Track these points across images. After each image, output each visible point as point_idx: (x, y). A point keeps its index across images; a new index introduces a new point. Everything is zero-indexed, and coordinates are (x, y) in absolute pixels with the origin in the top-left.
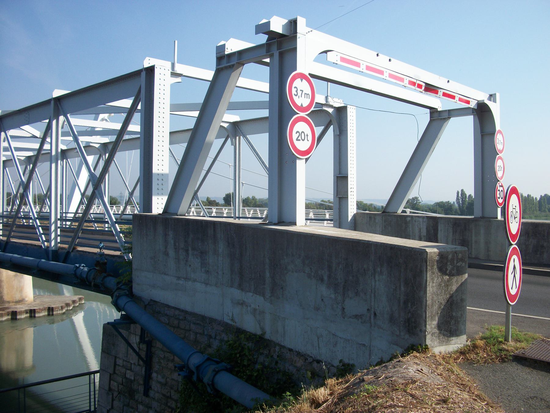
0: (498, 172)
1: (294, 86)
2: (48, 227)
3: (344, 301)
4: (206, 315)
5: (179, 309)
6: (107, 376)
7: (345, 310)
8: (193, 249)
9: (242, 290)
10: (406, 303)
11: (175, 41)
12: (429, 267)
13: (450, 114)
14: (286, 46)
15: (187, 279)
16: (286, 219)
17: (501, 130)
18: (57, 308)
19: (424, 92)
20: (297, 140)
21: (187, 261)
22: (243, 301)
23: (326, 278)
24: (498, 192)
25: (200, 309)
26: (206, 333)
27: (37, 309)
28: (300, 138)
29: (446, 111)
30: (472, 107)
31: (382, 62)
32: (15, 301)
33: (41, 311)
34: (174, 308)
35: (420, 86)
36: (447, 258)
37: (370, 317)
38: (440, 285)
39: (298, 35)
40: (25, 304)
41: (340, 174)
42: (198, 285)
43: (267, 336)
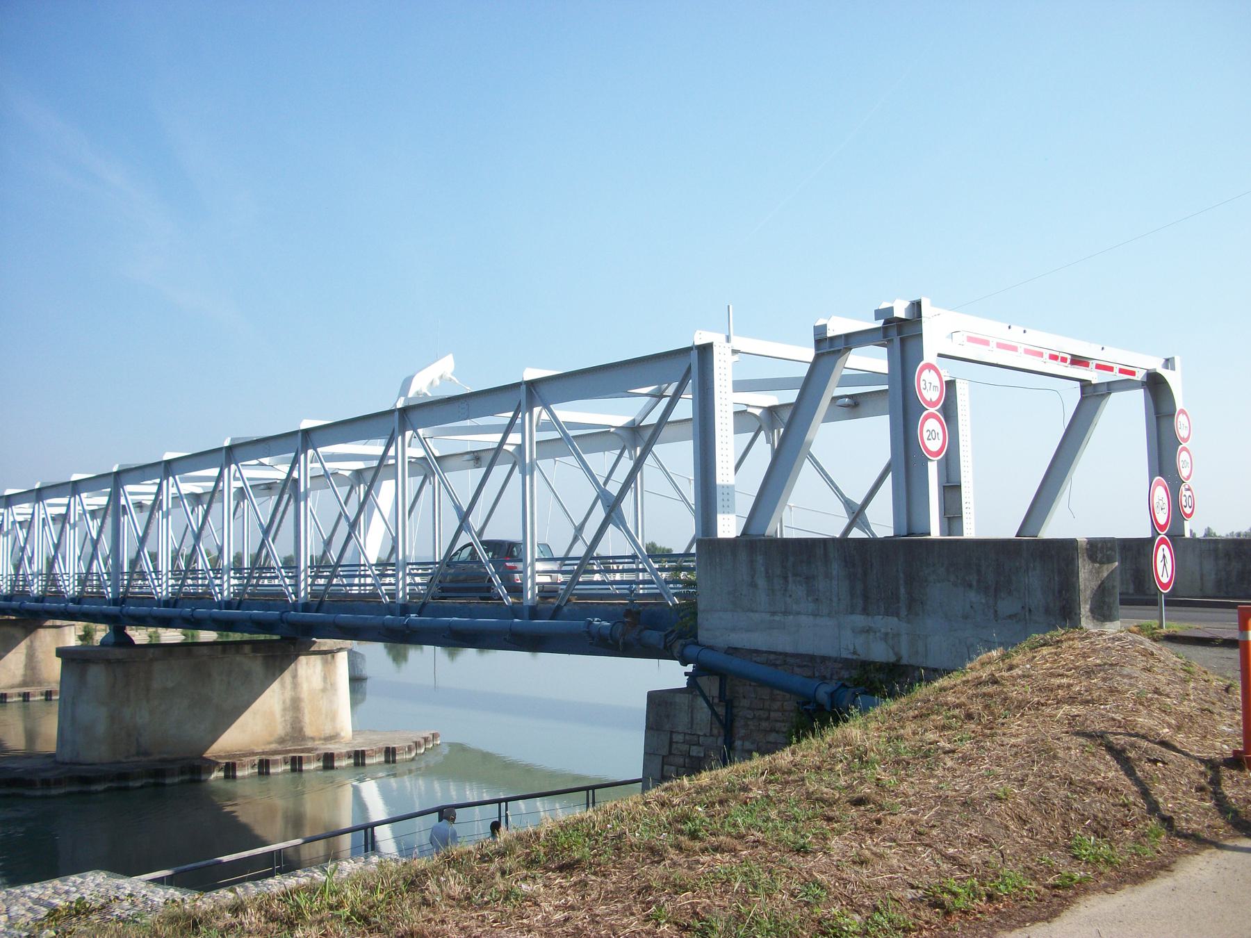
0: (1182, 469)
1: (921, 380)
2: (395, 594)
3: (996, 603)
4: (815, 654)
5: (774, 653)
6: (658, 760)
7: (998, 613)
8: (795, 575)
9: (868, 614)
10: (1060, 592)
11: (729, 307)
12: (1080, 555)
13: (1110, 387)
14: (908, 332)
15: (785, 613)
16: (916, 529)
17: (1185, 409)
18: (401, 750)
19: (1070, 365)
20: (929, 439)
21: (786, 590)
22: (870, 627)
23: (974, 583)
24: (1184, 499)
25: (806, 648)
26: (817, 674)
27: (367, 751)
28: (930, 437)
29: (1104, 383)
30: (1139, 379)
31: (1015, 336)
32: (323, 736)
33: (374, 754)
34: (766, 652)
35: (1064, 360)
36: (1097, 547)
37: (1025, 615)
38: (1091, 572)
39: (923, 319)
40: (341, 742)
41: (948, 482)
42: (803, 619)
43: (904, 661)
